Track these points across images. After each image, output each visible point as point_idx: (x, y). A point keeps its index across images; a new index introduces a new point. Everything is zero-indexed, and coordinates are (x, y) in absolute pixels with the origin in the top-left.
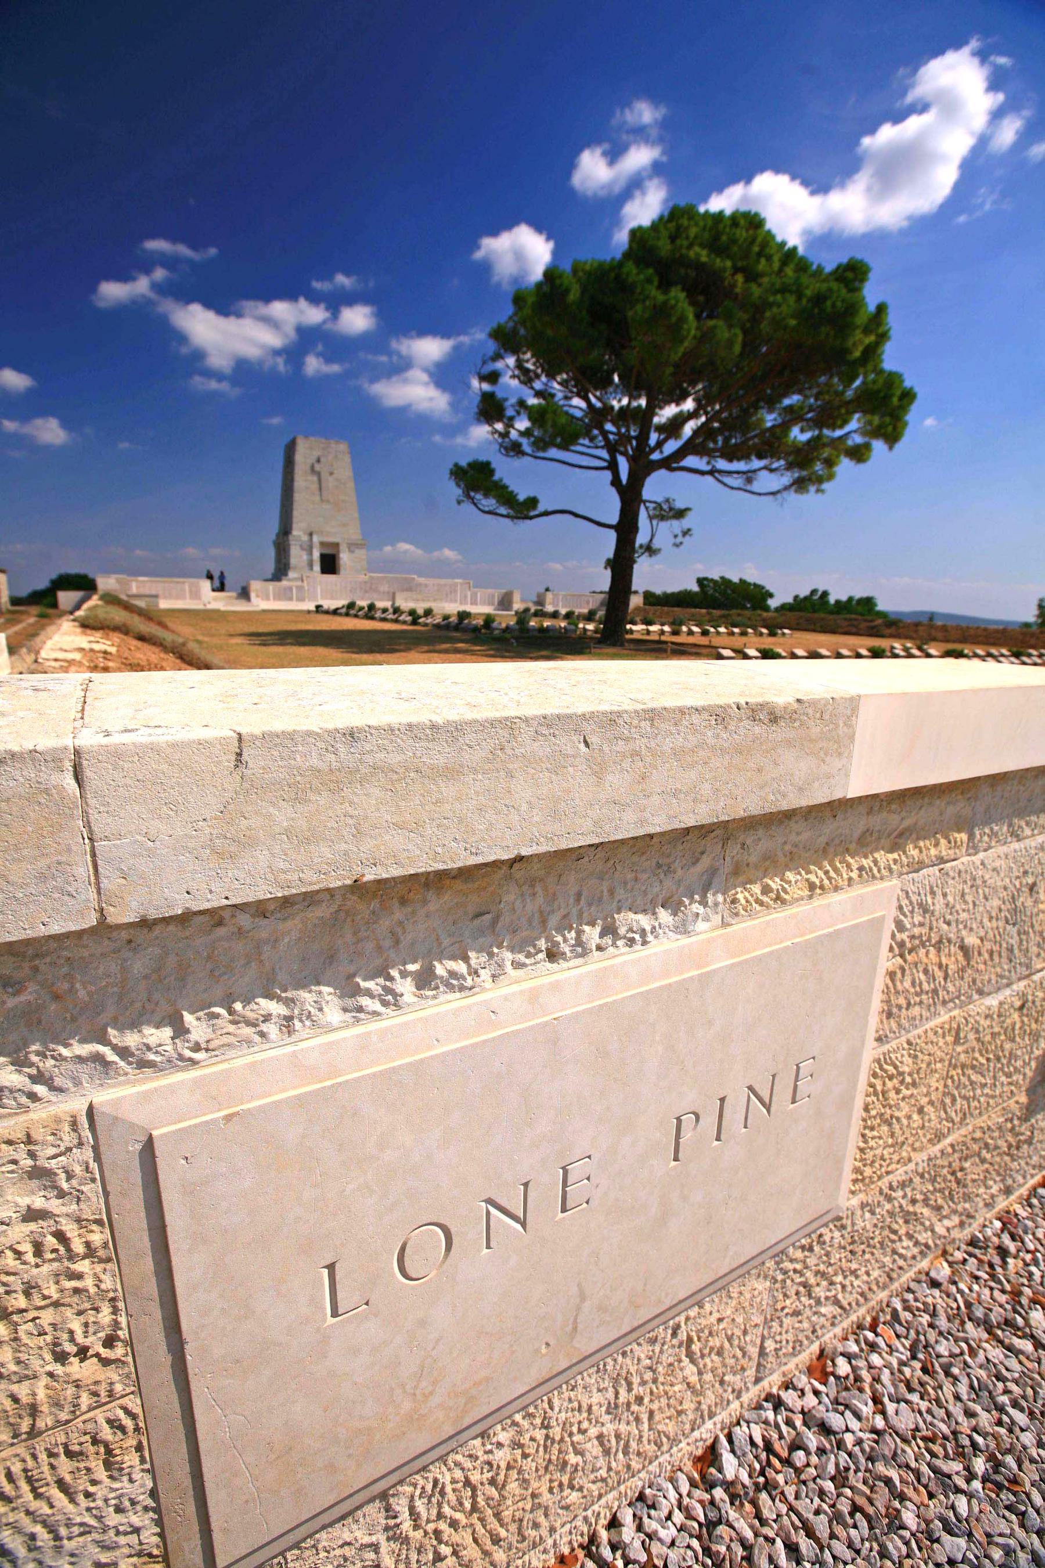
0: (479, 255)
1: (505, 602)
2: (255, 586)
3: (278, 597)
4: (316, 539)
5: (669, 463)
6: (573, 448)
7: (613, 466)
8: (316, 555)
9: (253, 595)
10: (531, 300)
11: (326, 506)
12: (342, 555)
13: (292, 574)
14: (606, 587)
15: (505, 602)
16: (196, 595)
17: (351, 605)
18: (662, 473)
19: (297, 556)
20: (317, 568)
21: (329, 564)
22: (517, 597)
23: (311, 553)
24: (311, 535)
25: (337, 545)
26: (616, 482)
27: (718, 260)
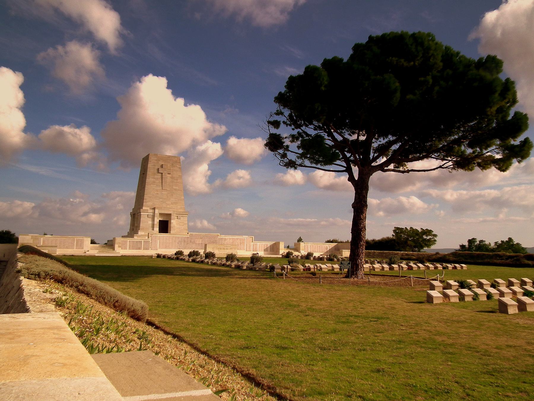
0: (472, 36)
1: (274, 248)
2: (119, 240)
3: (132, 247)
4: (157, 211)
5: (382, 167)
6: (335, 163)
7: (349, 170)
8: (157, 221)
9: (116, 246)
10: (488, 76)
11: (165, 193)
12: (172, 221)
13: (140, 233)
14: (350, 240)
15: (274, 248)
16: (80, 245)
17: (179, 253)
18: (379, 173)
19: (145, 221)
20: (157, 229)
21: (164, 227)
22: (282, 245)
23: (153, 220)
24: (154, 209)
25: (170, 215)
26: (351, 178)
27: (323, 73)
